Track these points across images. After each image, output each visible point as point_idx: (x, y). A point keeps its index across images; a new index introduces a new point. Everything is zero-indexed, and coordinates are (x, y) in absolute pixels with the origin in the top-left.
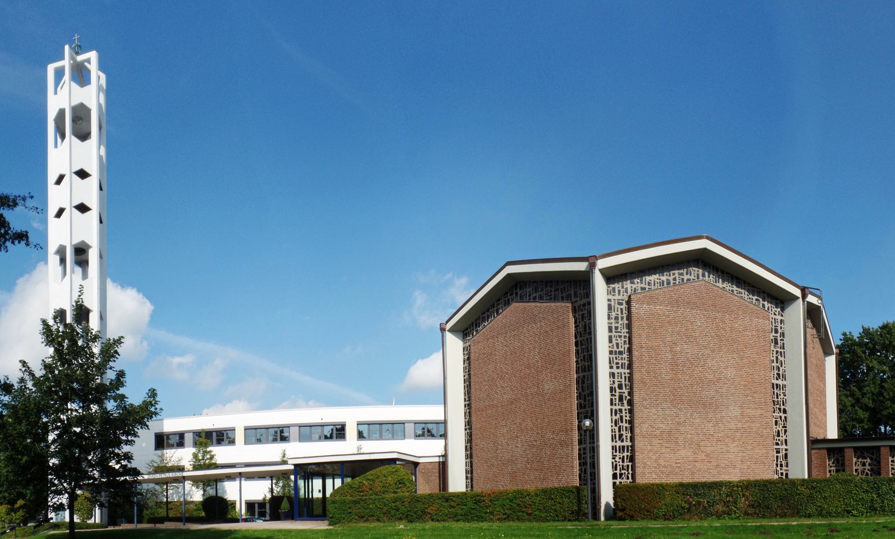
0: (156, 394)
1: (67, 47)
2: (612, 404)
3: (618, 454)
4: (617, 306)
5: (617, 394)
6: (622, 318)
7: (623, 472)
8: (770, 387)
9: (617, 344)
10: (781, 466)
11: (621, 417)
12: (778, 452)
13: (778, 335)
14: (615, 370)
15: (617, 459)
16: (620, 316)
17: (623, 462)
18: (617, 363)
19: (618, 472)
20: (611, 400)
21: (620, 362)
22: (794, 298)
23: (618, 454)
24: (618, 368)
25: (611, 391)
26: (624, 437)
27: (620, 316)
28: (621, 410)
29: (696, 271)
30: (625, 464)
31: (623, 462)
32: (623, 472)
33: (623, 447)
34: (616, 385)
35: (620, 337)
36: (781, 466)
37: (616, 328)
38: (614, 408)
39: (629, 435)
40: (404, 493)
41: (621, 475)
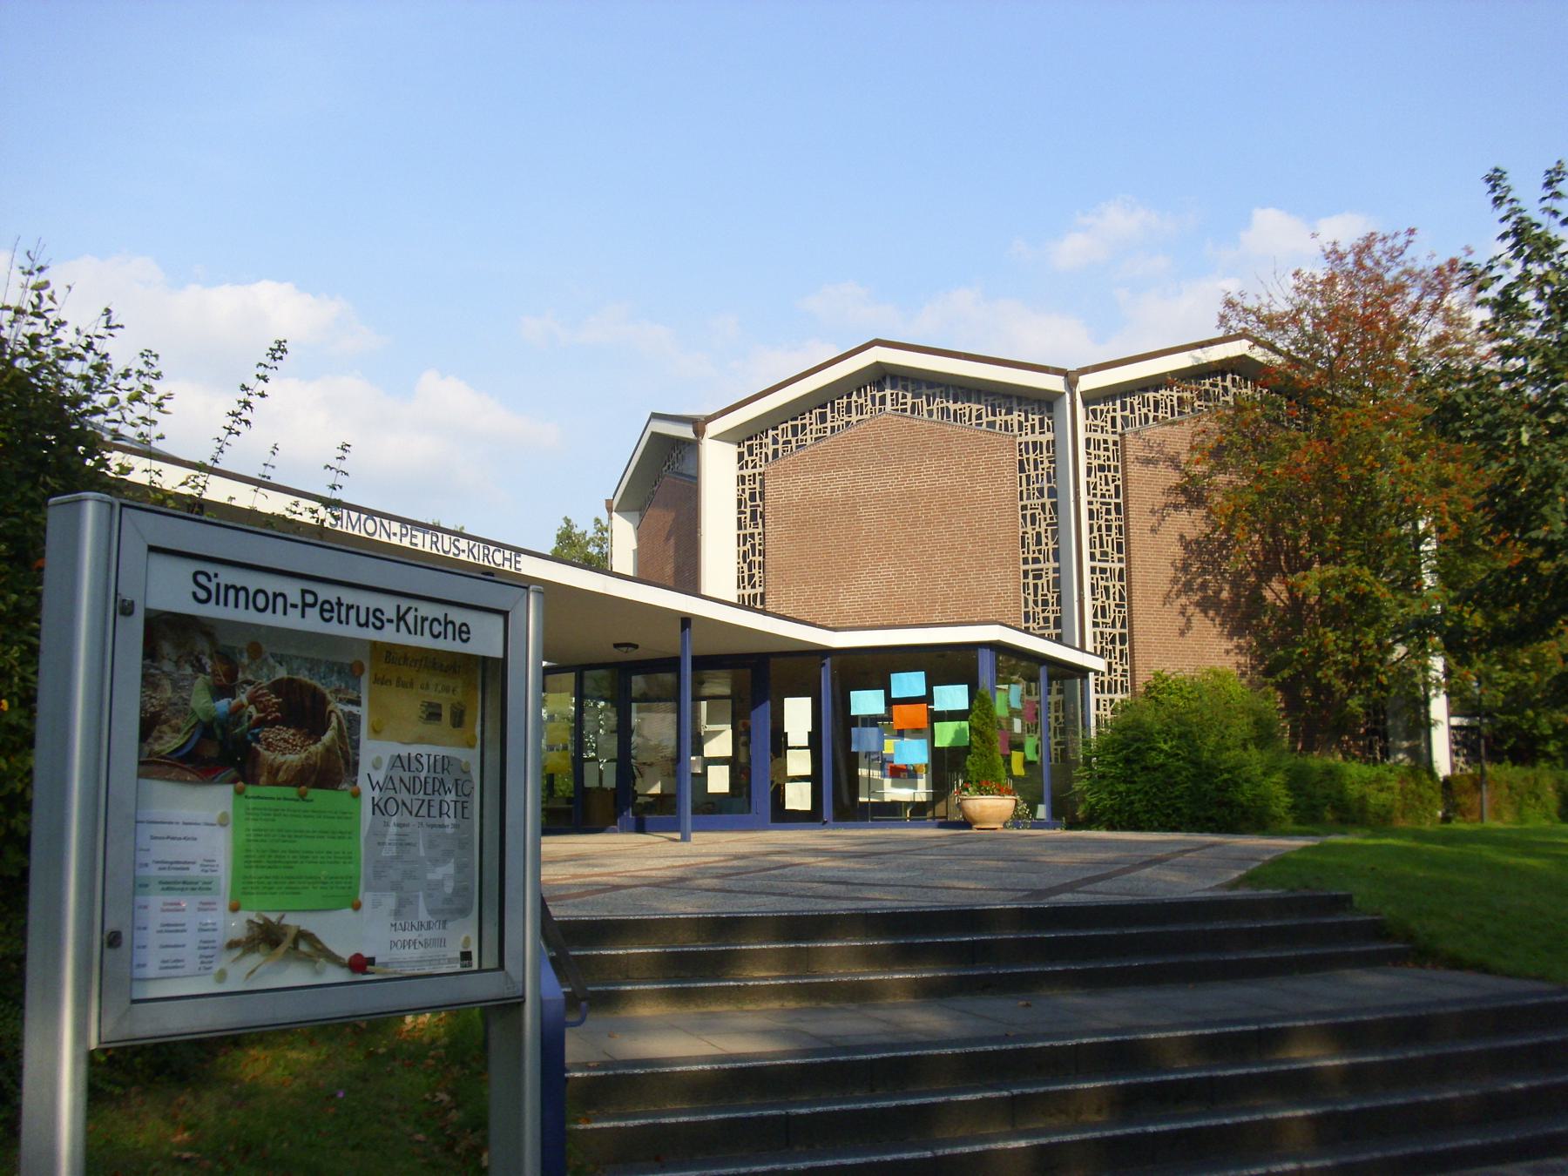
2: (740, 528)
3: (1119, 679)
4: (1109, 550)
5: (748, 511)
6: (1109, 528)
8: (822, 444)
10: (1045, 603)
11: (753, 546)
12: (1038, 577)
14: (746, 472)
16: (1104, 532)
18: (1106, 449)
20: (739, 520)
21: (1101, 453)
23: (1119, 679)
24: (1105, 442)
25: (739, 506)
26: (756, 579)
27: (1104, 532)
28: (752, 536)
29: (876, 348)
33: (1109, 691)
34: (747, 495)
35: (1103, 496)
36: (1045, 603)
37: (1108, 512)
38: (742, 532)
41: (1113, 641)
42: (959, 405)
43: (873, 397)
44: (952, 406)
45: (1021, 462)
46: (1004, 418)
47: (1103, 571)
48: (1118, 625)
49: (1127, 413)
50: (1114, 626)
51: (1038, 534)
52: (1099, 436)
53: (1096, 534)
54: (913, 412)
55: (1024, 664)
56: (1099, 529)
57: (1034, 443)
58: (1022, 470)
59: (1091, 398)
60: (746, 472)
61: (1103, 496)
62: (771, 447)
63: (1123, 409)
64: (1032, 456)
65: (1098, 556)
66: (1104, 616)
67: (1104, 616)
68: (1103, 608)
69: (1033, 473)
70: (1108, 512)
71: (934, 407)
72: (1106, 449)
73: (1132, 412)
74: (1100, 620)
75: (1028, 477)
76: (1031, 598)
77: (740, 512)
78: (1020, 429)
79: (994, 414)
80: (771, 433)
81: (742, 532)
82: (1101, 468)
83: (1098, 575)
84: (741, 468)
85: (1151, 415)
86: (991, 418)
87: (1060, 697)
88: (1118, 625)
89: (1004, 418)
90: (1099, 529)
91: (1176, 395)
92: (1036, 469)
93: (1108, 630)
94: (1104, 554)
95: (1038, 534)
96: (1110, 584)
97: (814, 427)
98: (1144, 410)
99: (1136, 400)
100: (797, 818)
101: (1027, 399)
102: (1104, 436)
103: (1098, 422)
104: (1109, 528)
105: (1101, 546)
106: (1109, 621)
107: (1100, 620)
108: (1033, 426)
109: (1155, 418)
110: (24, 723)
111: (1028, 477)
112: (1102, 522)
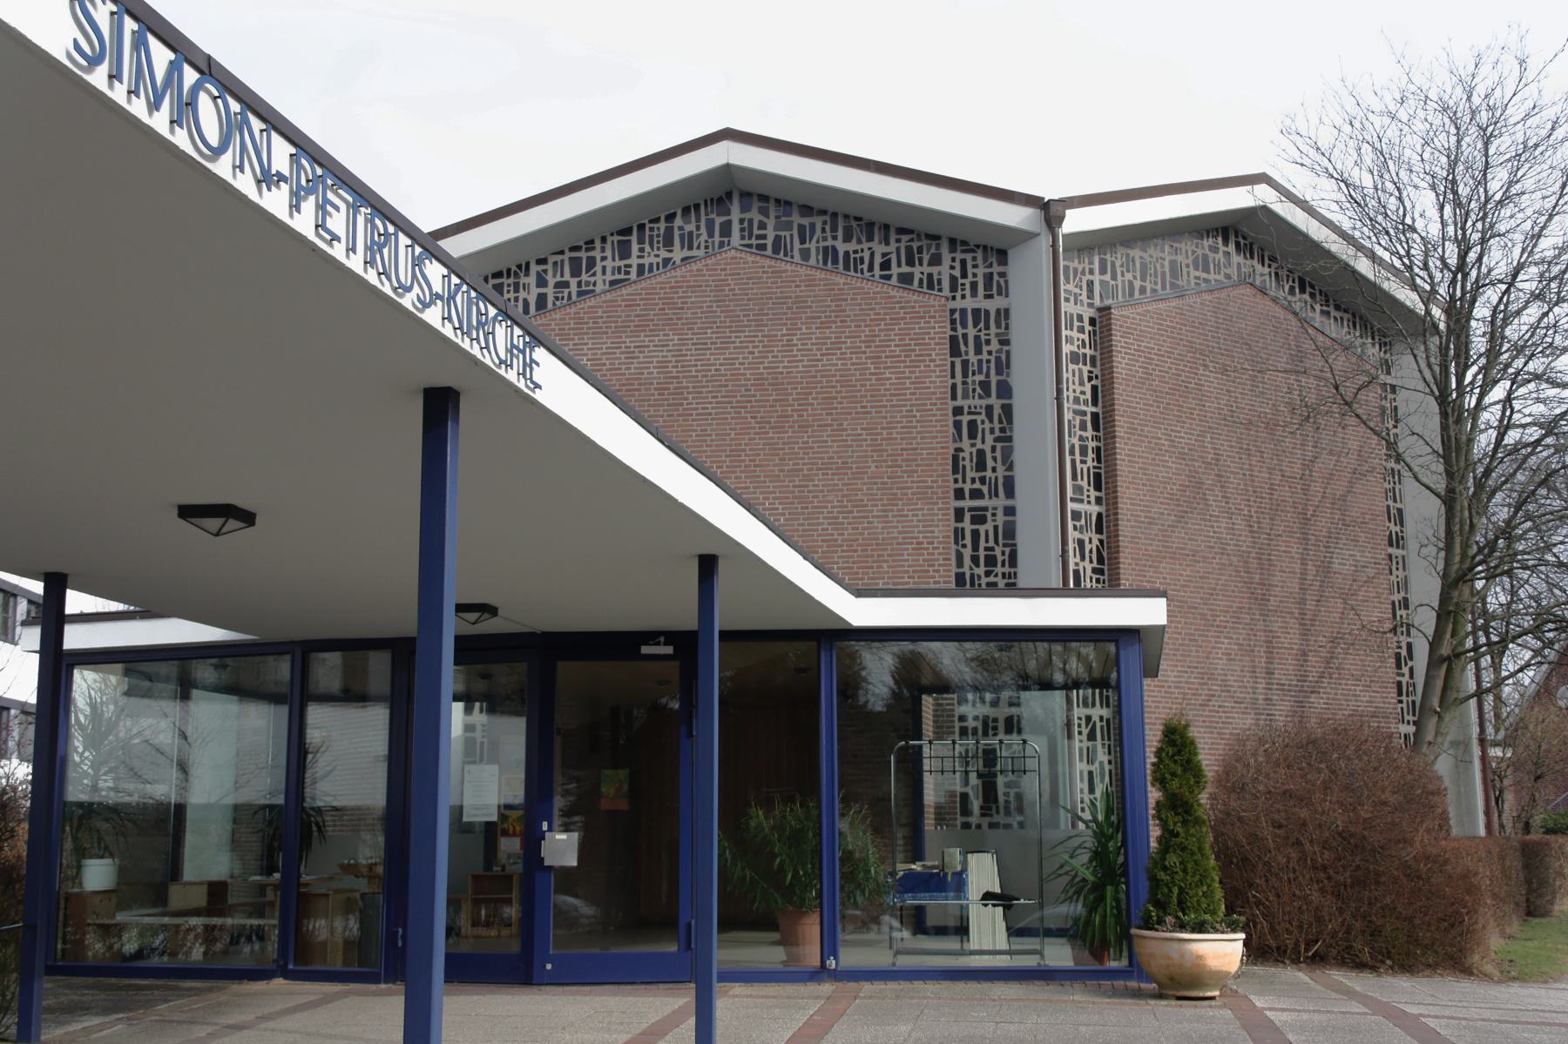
27: (1078, 457)
37: (1083, 427)
42: (852, 246)
46: (927, 269)
51: (981, 453)
57: (976, 312)
61: (1077, 400)
64: (971, 332)
69: (973, 358)
71: (812, 246)
75: (965, 364)
76: (967, 553)
79: (910, 263)
85: (1137, 284)
92: (978, 351)
95: (981, 453)
98: (1129, 276)
109: (1143, 290)
111: (965, 364)
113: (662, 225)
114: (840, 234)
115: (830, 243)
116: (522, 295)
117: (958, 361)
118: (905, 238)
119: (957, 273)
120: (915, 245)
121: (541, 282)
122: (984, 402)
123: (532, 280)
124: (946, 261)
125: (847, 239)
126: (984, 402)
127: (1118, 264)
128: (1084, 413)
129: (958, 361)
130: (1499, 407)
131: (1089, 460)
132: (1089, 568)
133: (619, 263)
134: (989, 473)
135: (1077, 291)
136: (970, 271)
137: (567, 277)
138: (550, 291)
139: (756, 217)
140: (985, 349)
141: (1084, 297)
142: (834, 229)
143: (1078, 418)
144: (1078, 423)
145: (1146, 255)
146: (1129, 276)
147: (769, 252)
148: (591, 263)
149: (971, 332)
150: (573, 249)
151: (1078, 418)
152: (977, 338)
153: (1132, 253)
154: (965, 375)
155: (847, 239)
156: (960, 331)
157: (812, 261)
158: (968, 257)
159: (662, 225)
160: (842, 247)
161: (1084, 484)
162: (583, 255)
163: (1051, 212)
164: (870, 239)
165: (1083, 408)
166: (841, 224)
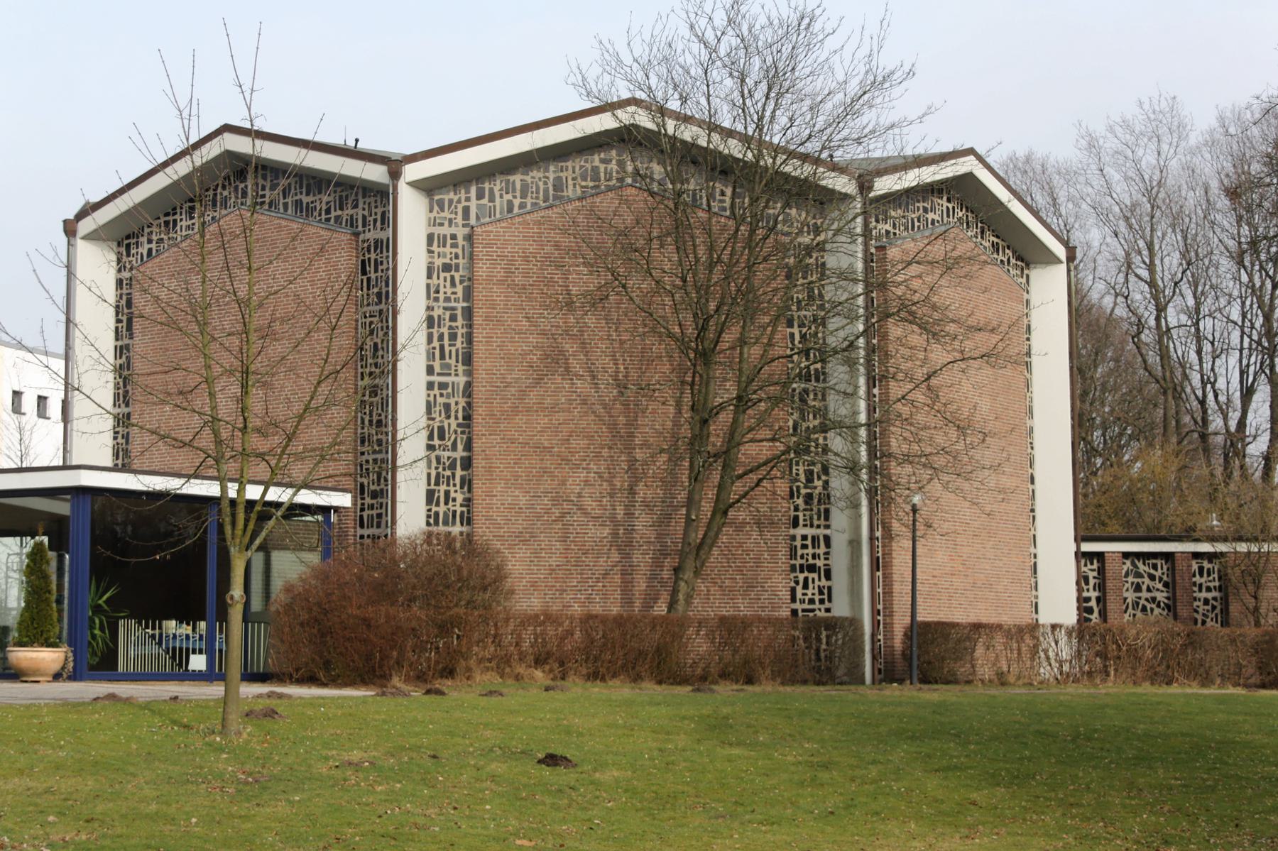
0: (66, 232)
1: (343, 500)
3: (459, 509)
5: (124, 319)
6: (453, 337)
7: (448, 473)
9: (453, 284)
13: (803, 491)
15: (460, 498)
16: (446, 342)
17: (447, 493)
19: (459, 473)
20: (117, 328)
21: (448, 249)
22: (1052, 259)
23: (459, 509)
24: (454, 237)
27: (446, 342)
29: (226, 135)
30: (443, 488)
31: (447, 493)
32: (448, 473)
33: (446, 523)
37: (453, 318)
39: (797, 162)
40: (547, 667)
41: (452, 466)
42: (310, 198)
43: (236, 188)
44: (305, 199)
45: (363, 261)
46: (350, 212)
47: (443, 386)
48: (460, 447)
49: (485, 201)
50: (454, 448)
51: (376, 344)
52: (446, 230)
53: (436, 344)
54: (270, 206)
55: (894, 445)
56: (441, 338)
57: (376, 241)
58: (364, 272)
59: (429, 187)
60: (126, 275)
61: (447, 299)
62: (147, 246)
63: (480, 196)
64: (373, 256)
65: (437, 369)
66: (442, 437)
67: (442, 437)
68: (441, 429)
69: (373, 276)
70: (453, 318)
71: (289, 200)
72: (454, 246)
73: (492, 200)
74: (436, 442)
75: (369, 279)
76: (367, 419)
77: (118, 321)
78: (364, 226)
79: (341, 209)
80: (147, 230)
81: (119, 343)
82: (447, 268)
83: (436, 391)
84: (119, 271)
85: (517, 202)
86: (339, 213)
87: (465, 529)
88: (460, 447)
89: (350, 212)
90: (441, 338)
91: (552, 176)
92: (376, 271)
93: (447, 454)
94: (443, 366)
95: (376, 344)
96: (452, 401)
97: (184, 223)
98: (509, 197)
99: (497, 186)
100: (197, 677)
101: (371, 190)
102: (453, 230)
103: (446, 214)
104: (453, 337)
105: (442, 357)
106: (449, 444)
107: (436, 442)
108: (375, 221)
109: (522, 206)
110: (283, 509)
111: (369, 279)
112: (445, 331)
113: (211, 193)
114: (304, 190)
115: (298, 197)
116: (140, 250)
117: (365, 278)
118: (339, 189)
119: (366, 213)
120: (344, 194)
121: (150, 241)
122: (378, 308)
123: (144, 239)
124: (361, 205)
125: (308, 194)
126: (378, 308)
127: (496, 189)
128: (453, 309)
129: (365, 278)
130: (207, 430)
131: (459, 343)
132: (454, 427)
133: (190, 223)
134: (380, 360)
135: (453, 216)
136: (374, 210)
137: (602, 167)
138: (153, 246)
139: (261, 181)
140: (380, 268)
141: (459, 220)
142: (301, 187)
143: (448, 313)
144: (447, 317)
145: (528, 179)
146: (509, 197)
147: (266, 207)
148: (175, 221)
149: (373, 256)
150: (167, 215)
151: (448, 313)
152: (376, 260)
153: (511, 178)
154: (368, 289)
155: (308, 194)
156: (367, 256)
157: (289, 212)
158: (372, 199)
159: (211, 193)
160: (305, 199)
161: (453, 362)
162: (171, 218)
163: (394, 165)
164: (320, 193)
165: (453, 304)
166: (305, 182)
